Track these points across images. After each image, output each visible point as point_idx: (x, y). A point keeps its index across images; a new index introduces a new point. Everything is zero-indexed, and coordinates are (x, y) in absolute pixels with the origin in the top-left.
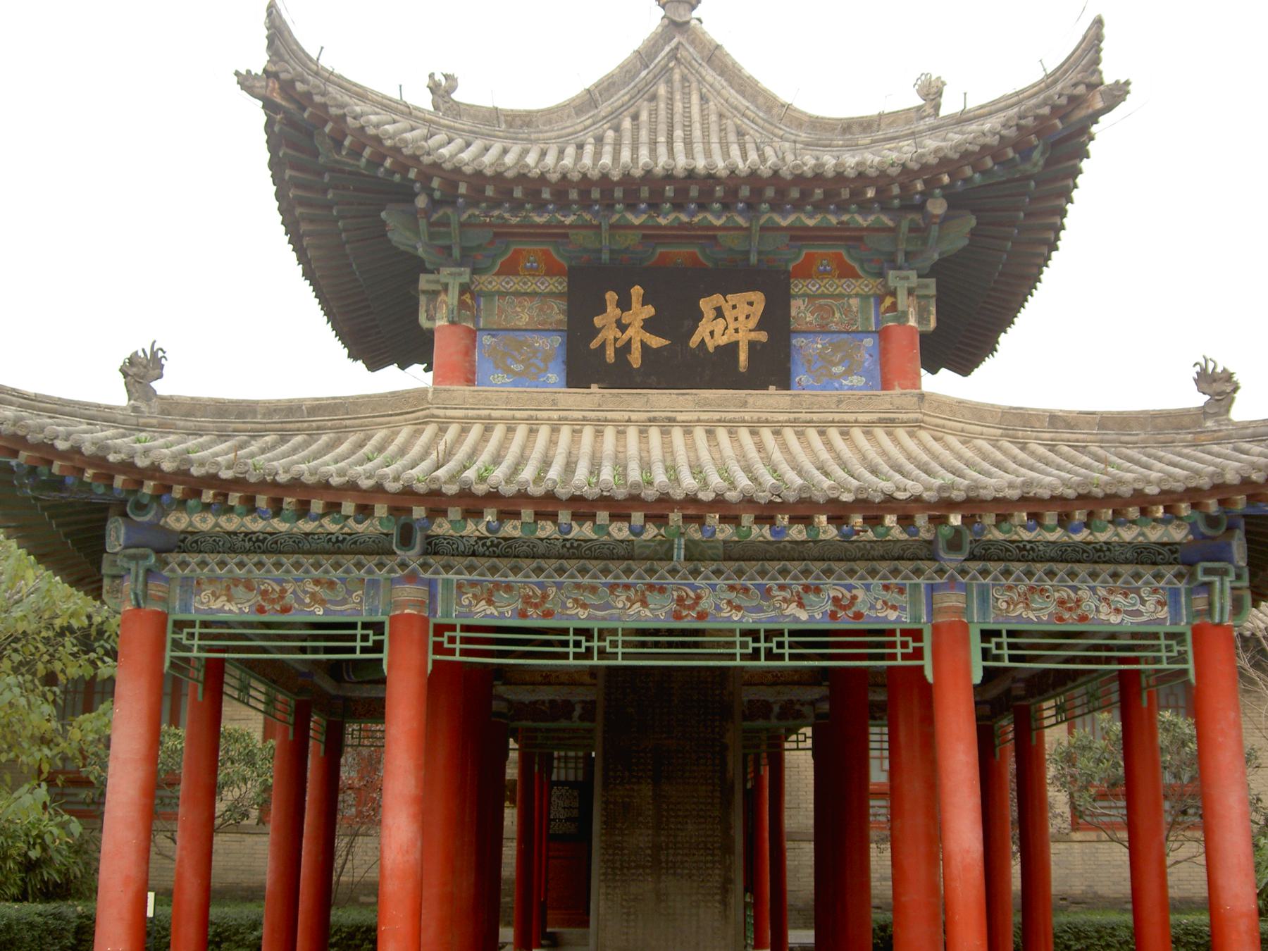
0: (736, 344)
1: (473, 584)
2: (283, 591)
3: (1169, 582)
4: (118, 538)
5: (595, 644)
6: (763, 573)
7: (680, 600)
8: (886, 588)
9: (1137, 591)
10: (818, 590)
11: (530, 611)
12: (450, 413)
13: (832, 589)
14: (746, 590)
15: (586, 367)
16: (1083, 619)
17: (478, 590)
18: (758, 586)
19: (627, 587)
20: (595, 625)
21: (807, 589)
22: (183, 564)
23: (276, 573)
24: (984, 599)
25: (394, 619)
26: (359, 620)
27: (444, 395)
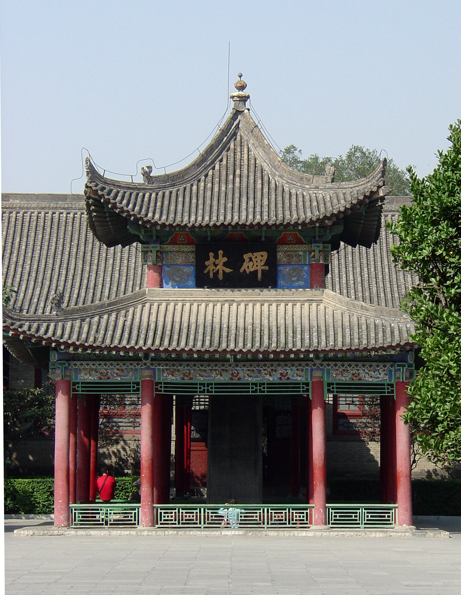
0: (257, 270)
1: (167, 369)
2: (107, 372)
3: (388, 368)
4: (55, 357)
5: (258, 388)
6: (258, 366)
7: (232, 374)
8: (298, 370)
9: (378, 371)
10: (276, 371)
11: (185, 378)
12: (154, 299)
13: (280, 370)
14: (253, 371)
15: (203, 280)
16: (360, 379)
17: (169, 372)
18: (257, 370)
19: (216, 370)
20: (206, 382)
21: (272, 370)
22: (75, 365)
23: (105, 367)
24: (328, 373)
25: (142, 381)
26: (132, 381)
27: (152, 292)
